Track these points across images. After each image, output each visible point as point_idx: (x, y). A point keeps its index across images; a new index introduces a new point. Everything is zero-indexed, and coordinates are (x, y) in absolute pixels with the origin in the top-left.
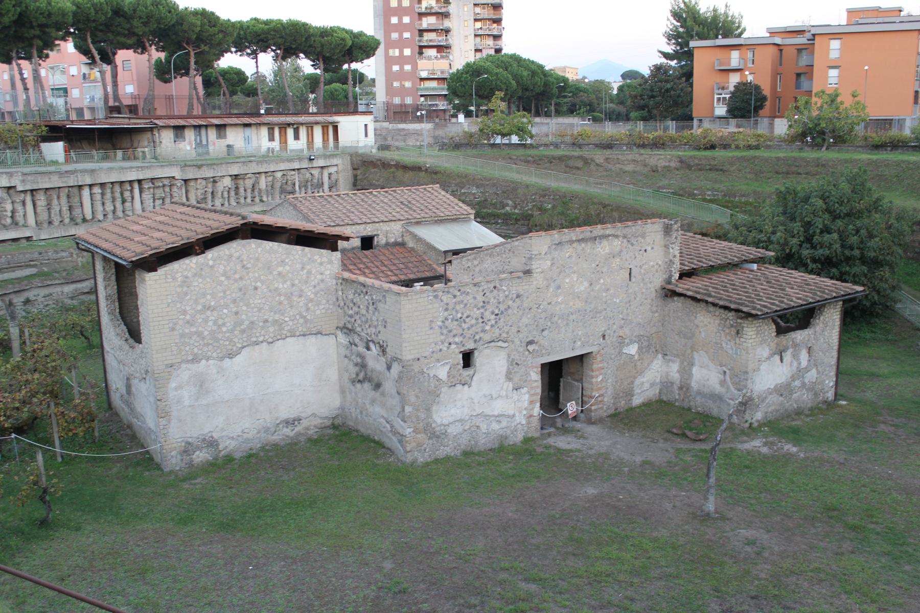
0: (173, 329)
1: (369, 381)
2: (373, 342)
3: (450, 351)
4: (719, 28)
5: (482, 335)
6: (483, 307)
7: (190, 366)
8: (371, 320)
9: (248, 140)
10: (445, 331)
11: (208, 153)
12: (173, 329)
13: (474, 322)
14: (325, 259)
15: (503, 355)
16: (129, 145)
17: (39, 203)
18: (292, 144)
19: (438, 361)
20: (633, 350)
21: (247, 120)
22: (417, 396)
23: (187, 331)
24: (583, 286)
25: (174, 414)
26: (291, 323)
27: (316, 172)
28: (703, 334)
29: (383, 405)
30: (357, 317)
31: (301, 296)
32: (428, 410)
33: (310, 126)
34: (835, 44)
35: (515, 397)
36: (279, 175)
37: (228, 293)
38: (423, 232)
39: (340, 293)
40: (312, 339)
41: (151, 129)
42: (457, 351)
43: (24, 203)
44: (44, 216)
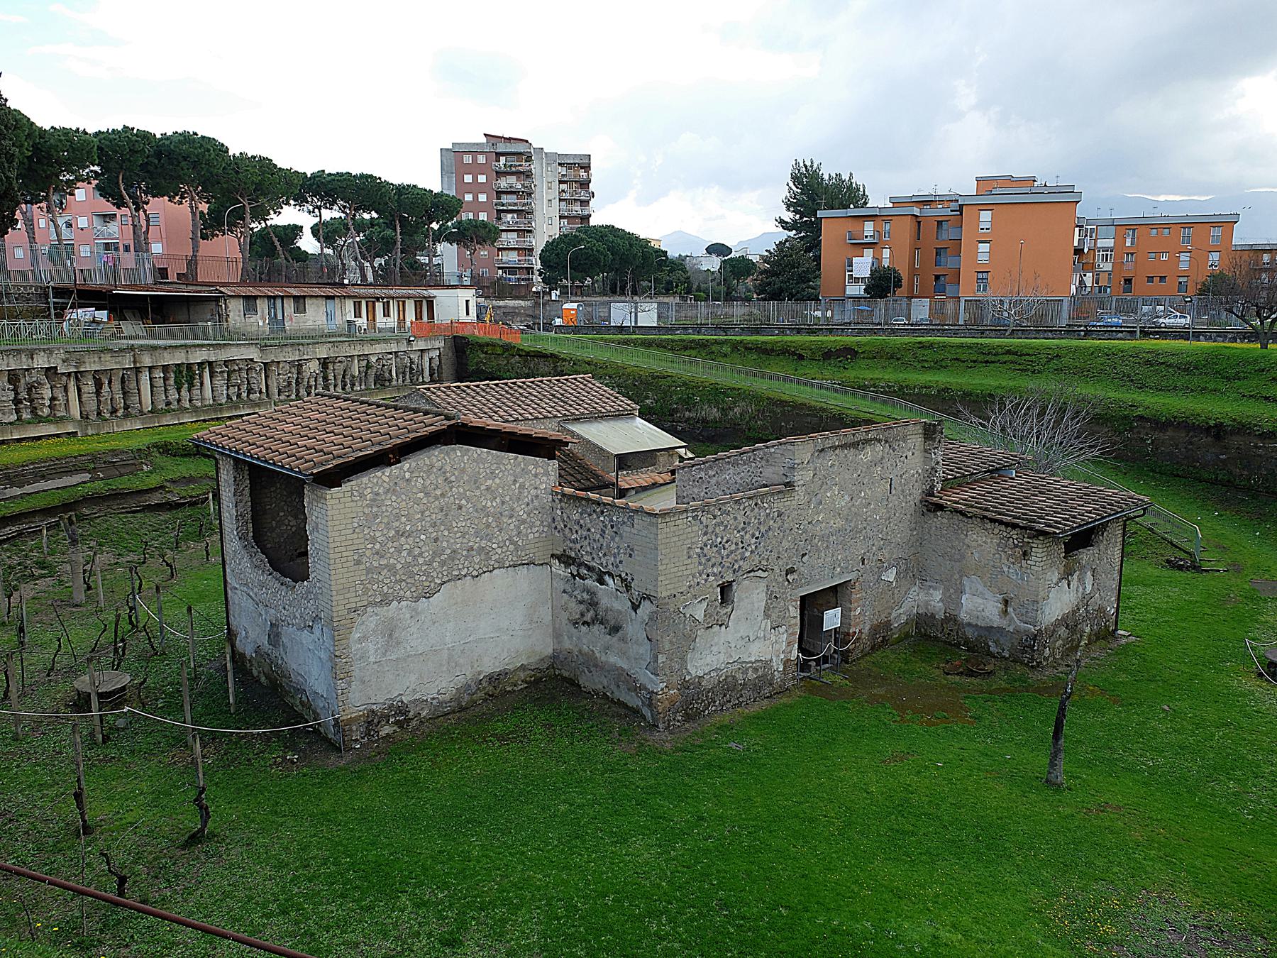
0: (358, 562)
1: (601, 623)
2: (610, 575)
3: (708, 585)
4: (845, 195)
5: (741, 563)
6: (743, 529)
7: (377, 609)
8: (608, 546)
9: (330, 316)
10: (703, 560)
11: (284, 330)
12: (358, 562)
13: (733, 547)
14: (540, 470)
15: (762, 586)
16: (185, 317)
17: (85, 389)
18: (381, 321)
19: (695, 597)
20: (891, 576)
21: (330, 291)
22: (671, 642)
23: (376, 564)
24: (844, 502)
25: (356, 673)
26: (499, 551)
27: (415, 357)
28: (976, 556)
29: (623, 654)
30: (585, 543)
31: (511, 517)
32: (683, 659)
33: (402, 301)
34: (986, 216)
35: (773, 638)
36: (373, 359)
37: (427, 513)
38: (576, 428)
39: (559, 512)
40: (524, 569)
41: (217, 299)
42: (715, 584)
43: (66, 389)
44: (92, 406)
